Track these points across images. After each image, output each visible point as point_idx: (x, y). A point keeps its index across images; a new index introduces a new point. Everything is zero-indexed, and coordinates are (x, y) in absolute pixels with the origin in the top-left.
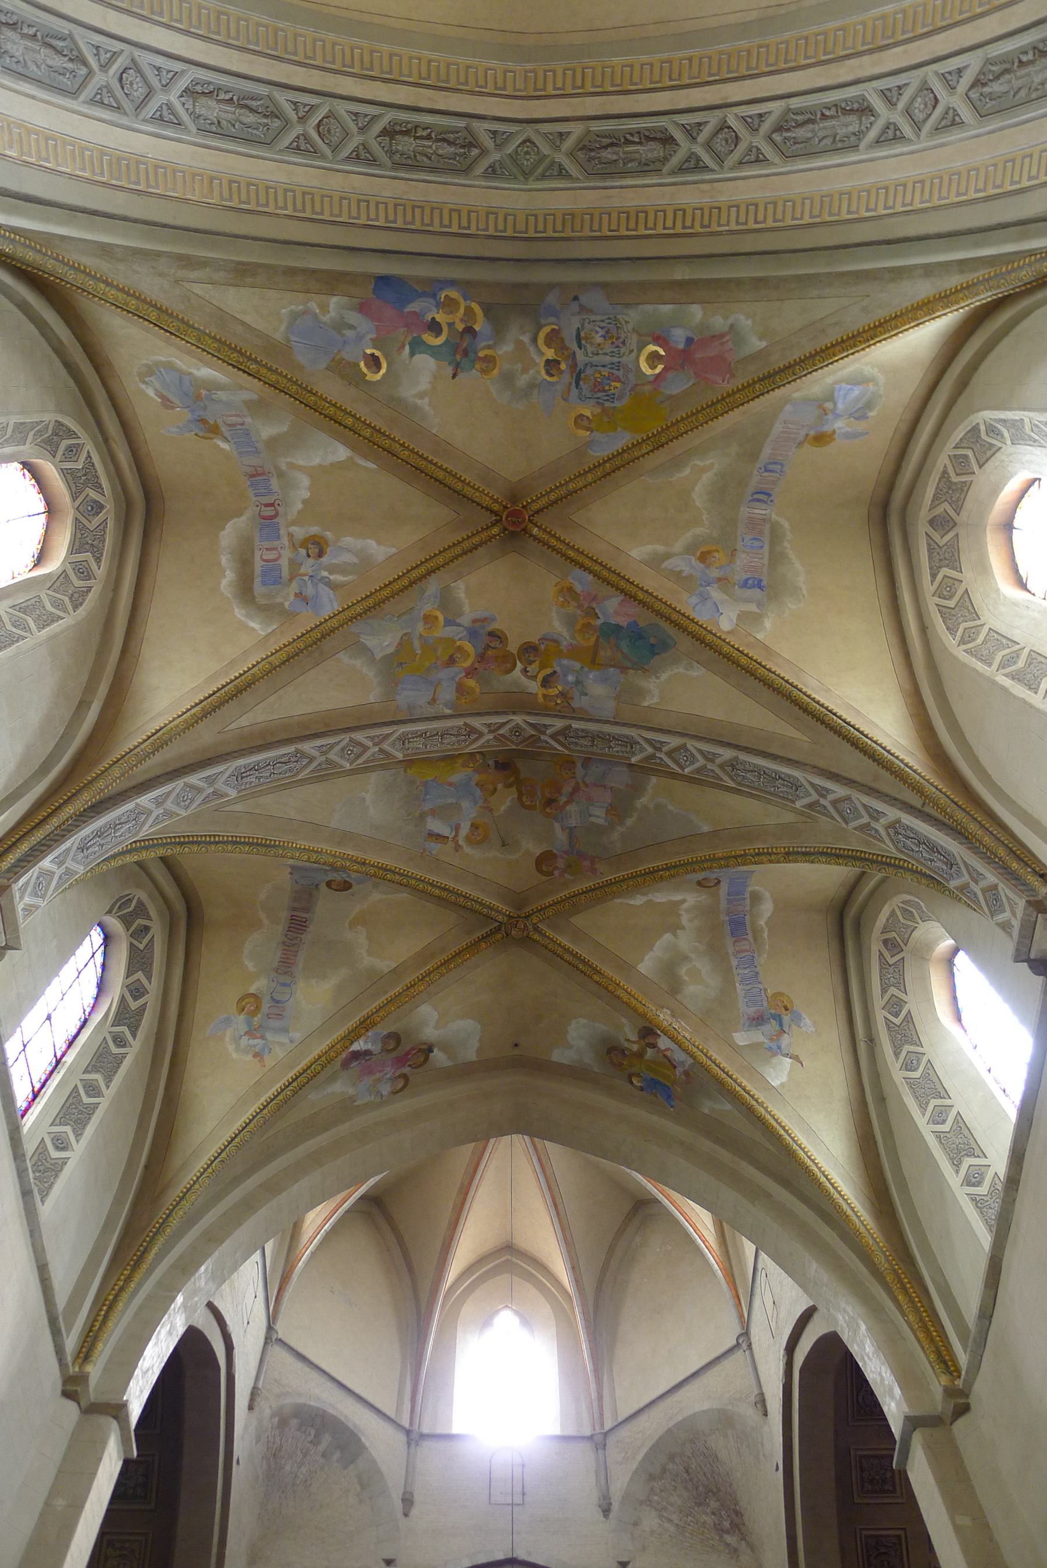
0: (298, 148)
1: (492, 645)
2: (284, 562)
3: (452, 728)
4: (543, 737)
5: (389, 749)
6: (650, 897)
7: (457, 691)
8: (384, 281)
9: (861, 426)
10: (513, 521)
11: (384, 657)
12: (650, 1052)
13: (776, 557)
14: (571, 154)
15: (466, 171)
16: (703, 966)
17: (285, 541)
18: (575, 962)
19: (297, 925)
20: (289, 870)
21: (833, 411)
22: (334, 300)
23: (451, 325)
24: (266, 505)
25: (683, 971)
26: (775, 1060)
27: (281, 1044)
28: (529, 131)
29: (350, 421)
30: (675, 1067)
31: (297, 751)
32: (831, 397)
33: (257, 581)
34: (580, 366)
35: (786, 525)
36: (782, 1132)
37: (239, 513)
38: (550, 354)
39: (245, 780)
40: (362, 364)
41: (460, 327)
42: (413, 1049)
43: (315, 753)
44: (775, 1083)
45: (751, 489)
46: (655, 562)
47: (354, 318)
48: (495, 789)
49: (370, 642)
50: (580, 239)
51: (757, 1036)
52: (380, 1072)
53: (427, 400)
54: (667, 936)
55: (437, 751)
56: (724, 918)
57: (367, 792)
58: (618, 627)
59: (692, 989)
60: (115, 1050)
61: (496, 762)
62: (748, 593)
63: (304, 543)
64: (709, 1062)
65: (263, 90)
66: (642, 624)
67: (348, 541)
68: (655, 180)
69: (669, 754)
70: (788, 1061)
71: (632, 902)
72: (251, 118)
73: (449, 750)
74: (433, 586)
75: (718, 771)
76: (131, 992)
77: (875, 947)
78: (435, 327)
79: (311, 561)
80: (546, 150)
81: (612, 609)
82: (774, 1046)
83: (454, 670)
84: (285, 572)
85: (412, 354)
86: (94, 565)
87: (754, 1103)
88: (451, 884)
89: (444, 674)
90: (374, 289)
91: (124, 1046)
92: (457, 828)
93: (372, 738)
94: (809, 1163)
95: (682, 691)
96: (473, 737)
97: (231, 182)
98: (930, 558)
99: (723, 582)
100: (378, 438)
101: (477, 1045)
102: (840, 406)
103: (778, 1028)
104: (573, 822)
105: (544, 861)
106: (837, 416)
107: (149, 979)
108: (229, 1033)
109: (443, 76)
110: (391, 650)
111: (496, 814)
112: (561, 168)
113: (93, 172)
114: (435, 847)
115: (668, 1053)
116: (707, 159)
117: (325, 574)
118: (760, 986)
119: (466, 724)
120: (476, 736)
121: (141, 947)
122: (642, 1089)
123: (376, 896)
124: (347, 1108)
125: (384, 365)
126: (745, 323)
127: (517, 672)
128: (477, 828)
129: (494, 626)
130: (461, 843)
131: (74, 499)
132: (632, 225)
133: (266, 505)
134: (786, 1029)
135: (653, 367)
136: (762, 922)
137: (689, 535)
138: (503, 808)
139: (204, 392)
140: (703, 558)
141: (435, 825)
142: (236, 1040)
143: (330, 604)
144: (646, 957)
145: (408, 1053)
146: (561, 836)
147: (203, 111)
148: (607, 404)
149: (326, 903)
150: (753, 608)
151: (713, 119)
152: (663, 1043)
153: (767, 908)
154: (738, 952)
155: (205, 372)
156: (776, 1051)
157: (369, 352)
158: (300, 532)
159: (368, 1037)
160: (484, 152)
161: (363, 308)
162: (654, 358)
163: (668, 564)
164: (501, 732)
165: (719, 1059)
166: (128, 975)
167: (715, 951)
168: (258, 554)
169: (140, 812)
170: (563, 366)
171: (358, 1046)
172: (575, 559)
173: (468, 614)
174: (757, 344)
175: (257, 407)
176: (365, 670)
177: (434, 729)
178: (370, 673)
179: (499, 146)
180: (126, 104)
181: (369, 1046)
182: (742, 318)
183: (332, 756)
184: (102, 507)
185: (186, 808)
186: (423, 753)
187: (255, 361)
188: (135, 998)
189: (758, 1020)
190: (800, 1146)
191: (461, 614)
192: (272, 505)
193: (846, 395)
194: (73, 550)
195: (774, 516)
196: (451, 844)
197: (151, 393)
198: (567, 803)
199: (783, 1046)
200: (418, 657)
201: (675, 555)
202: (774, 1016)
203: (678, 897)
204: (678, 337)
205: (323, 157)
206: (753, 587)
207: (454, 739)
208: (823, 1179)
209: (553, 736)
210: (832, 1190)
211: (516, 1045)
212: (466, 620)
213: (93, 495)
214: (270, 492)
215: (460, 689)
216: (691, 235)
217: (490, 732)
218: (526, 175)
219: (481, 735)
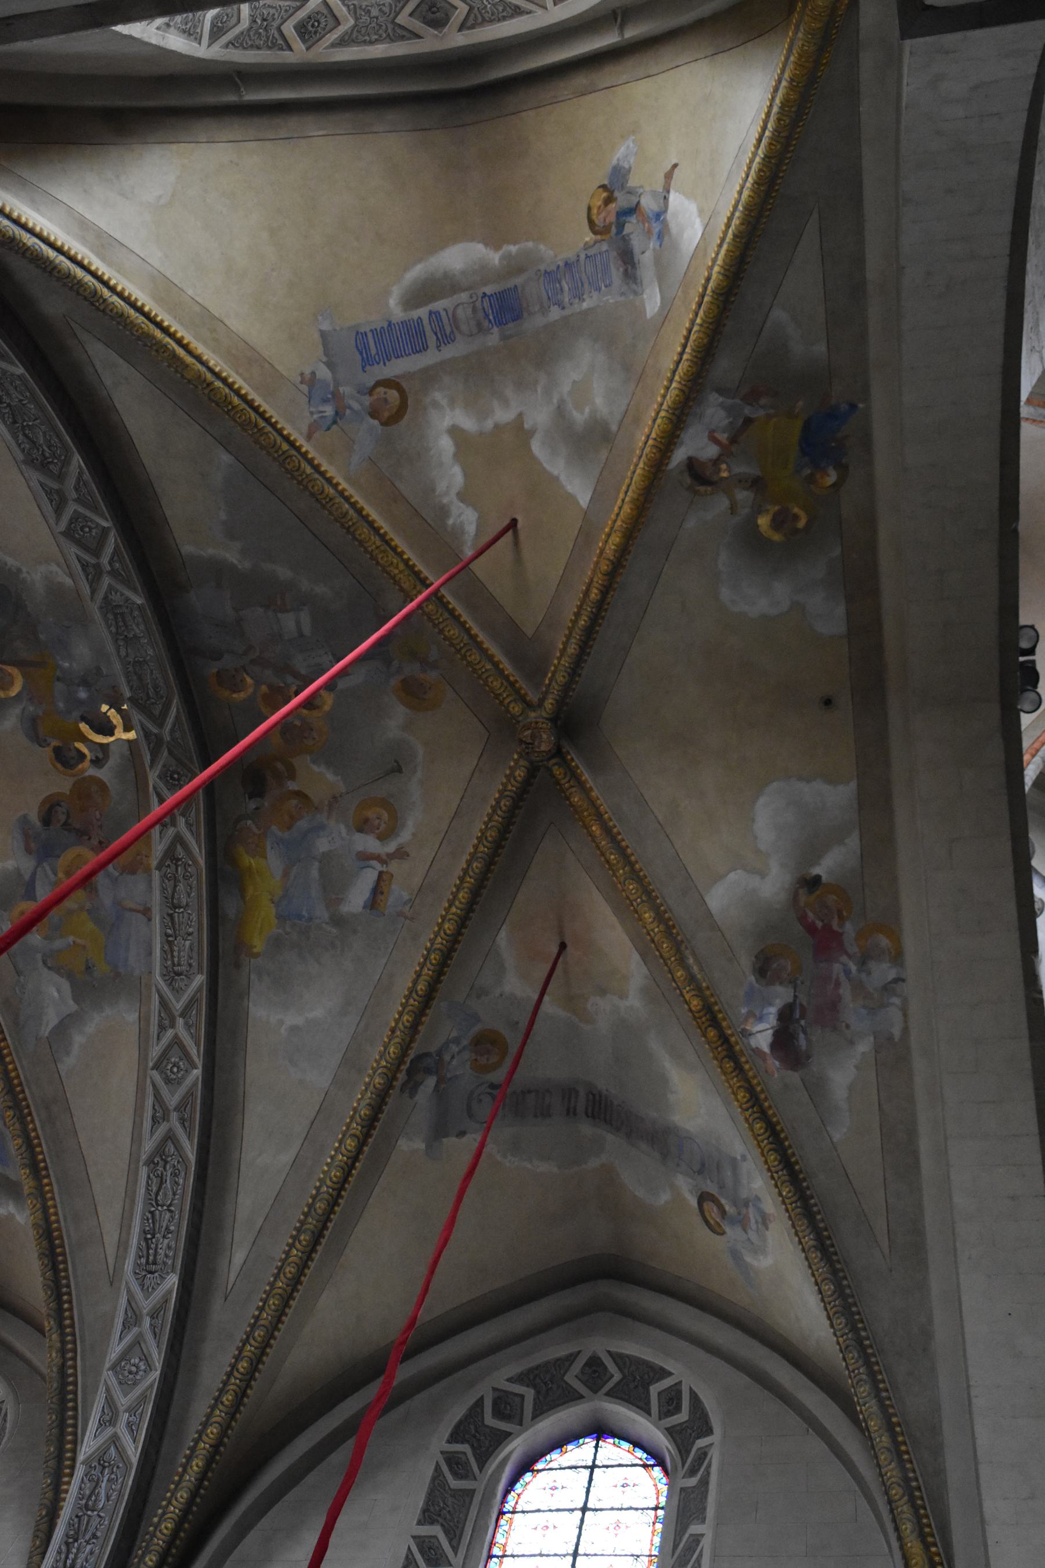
1: (63, 818)
3: (163, 890)
4: (167, 738)
5: (185, 998)
6: (450, 499)
11: (76, 999)
25: (580, 418)
30: (748, 421)
39: (160, 1258)
43: (162, 1130)
48: (298, 794)
49: (51, 1019)
52: (838, 984)
55: (200, 916)
56: (493, 338)
57: (281, 1022)
69: (97, 553)
73: (200, 896)
82: (656, 227)
92: (365, 857)
93: (162, 1028)
96: (180, 852)
101: (819, 786)
103: (633, 219)
110: (66, 986)
114: (398, 893)
115: (723, 437)
118: (583, 257)
120: (179, 847)
124: (893, 1057)
127: (103, 774)
128: (366, 821)
129: (34, 817)
130: (391, 847)
136: (495, 258)
138: (330, 776)
141: (356, 899)
144: (569, 488)
145: (811, 929)
149: (545, 1065)
152: (696, 444)
153: (458, 257)
159: (751, 1014)
166: (646, 1410)
167: (545, 354)
169: (100, 1461)
171: (762, 1036)
176: (90, 1028)
177: (162, 922)
178: (94, 1023)
181: (772, 1011)
185: (150, 1367)
186: (200, 942)
196: (394, 867)
200: (79, 941)
203: (446, 445)
207: (181, 887)
212: (26, 864)
219: (178, 839)
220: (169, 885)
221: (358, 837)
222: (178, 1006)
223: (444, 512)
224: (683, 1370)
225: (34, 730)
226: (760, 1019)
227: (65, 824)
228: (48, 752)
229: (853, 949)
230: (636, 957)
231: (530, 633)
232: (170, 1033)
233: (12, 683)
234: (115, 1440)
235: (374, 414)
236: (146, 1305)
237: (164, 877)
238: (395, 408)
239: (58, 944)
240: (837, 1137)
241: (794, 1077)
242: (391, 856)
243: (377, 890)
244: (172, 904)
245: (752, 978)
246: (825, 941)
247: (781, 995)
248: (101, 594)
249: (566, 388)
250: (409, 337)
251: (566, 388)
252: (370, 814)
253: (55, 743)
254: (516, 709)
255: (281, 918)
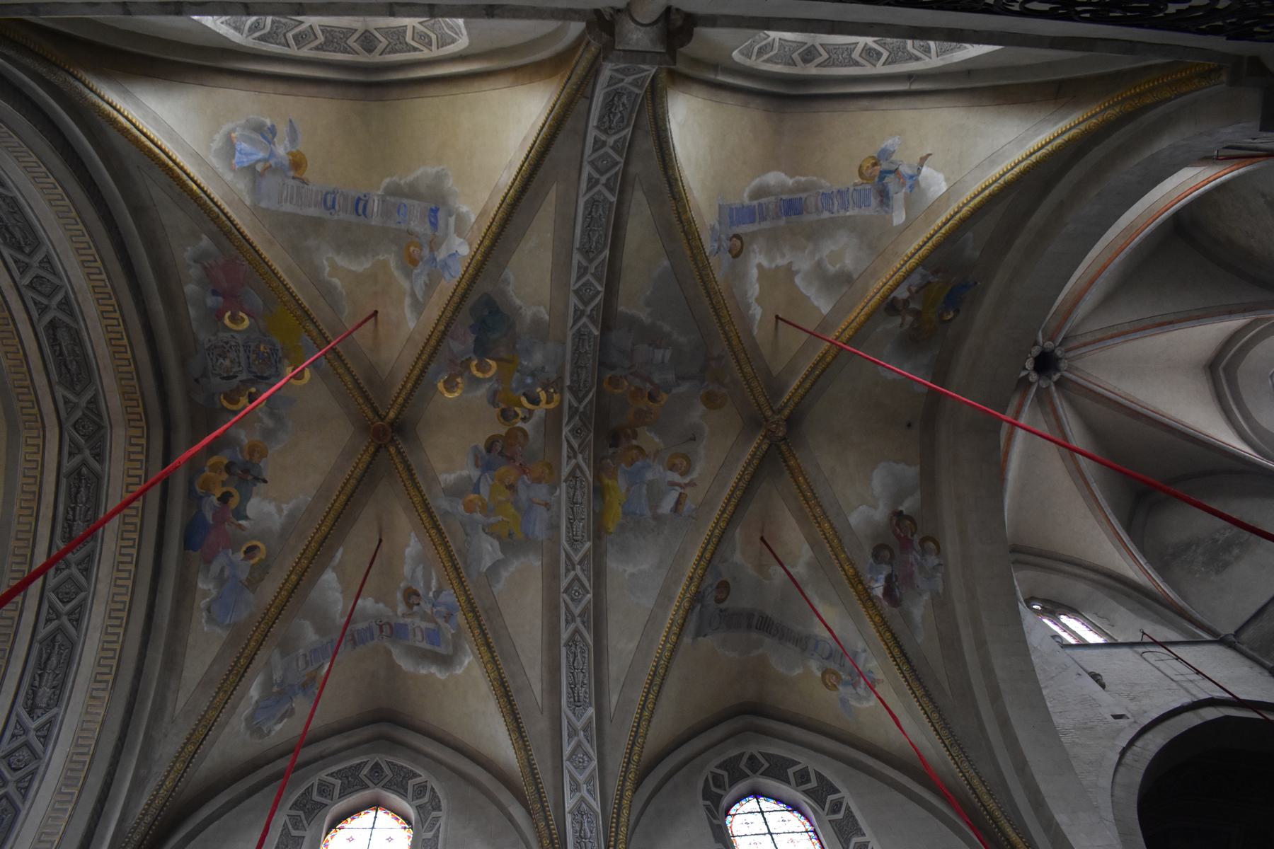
0: (77, 620)
2: (424, 625)
4: (581, 409)
5: (580, 554)
6: (752, 300)
7: (540, 482)
8: (189, 541)
9: (283, 129)
10: (386, 434)
11: (503, 550)
12: (912, 306)
13: (412, 192)
14: (78, 394)
15: (98, 478)
16: (828, 248)
17: (408, 620)
18: (812, 378)
19: (765, 625)
20: (700, 639)
21: (265, 160)
22: (201, 585)
23: (224, 484)
24: (381, 631)
25: (832, 269)
26: (923, 184)
27: (866, 659)
28: (68, 426)
29: (294, 577)
30: (929, 283)
31: (567, 645)
32: (251, 169)
33: (437, 649)
34: (251, 376)
35: (387, 180)
36: (987, 192)
37: (389, 653)
38: (244, 400)
40: (252, 562)
41: (225, 476)
42: (894, 531)
43: (572, 627)
44: (943, 187)
45: (353, 218)
46: (418, 307)
47: (215, 567)
48: (637, 447)
49: (487, 562)
50: (141, 387)
51: (898, 198)
53: (284, 506)
54: (798, 280)
58: (477, 341)
59: (849, 262)
60: (840, 816)
61: (611, 446)
62: (441, 223)
63: (410, 606)
64: (917, 256)
65: (36, 647)
66: (472, 322)
67: (407, 570)
68: (85, 334)
69: (586, 304)
70: (925, 170)
71: (758, 317)
72: (54, 660)
74: (441, 503)
75: (596, 263)
76: (802, 783)
77: (812, 70)
78: (225, 498)
79: (422, 603)
80: (79, 414)
81: (461, 344)
82: (909, 183)
83: (520, 486)
84: (431, 626)
85: (246, 518)
86: (418, 780)
87: (957, 217)
88: (728, 491)
89: (523, 495)
90: (194, 550)
91: (841, 804)
92: (673, 484)
93: (568, 571)
94: (1017, 170)
95: (532, 282)
96: (578, 473)
97: (96, 681)
98: (400, 51)
99: (434, 245)
100: (309, 554)
102: (261, 155)
103: (892, 176)
104: (671, 377)
105: (711, 401)
106: (272, 154)
107: (796, 763)
108: (853, 703)
109: (31, 497)
110: (496, 543)
111: (662, 446)
112: (90, 402)
113: (70, 802)
114: (689, 505)
115: (914, 289)
116: (59, 297)
117: (431, 594)
119: (566, 481)
121: (766, 765)
122: (957, 311)
123: (738, 557)
124: (941, 603)
125: (255, 543)
126: (189, 253)
127: (527, 427)
129: (482, 446)
130: (687, 480)
131: (367, 787)
132: (123, 349)
133: (381, 631)
134: (894, 167)
135: (243, 320)
136: (790, 182)
137: (396, 273)
138: (657, 440)
139: (275, 689)
140: (414, 262)
141: (667, 505)
142: (859, 698)
143: (449, 597)
144: (816, 303)
145: (898, 537)
146: (684, 388)
147: (45, 700)
148: (280, 354)
149: (741, 601)
150: (452, 220)
151: (29, 294)
152: (902, 293)
153: (774, 178)
154: (817, 209)
155: (254, 693)
156: (914, 177)
157: (242, 556)
158: (401, 608)
160: (84, 463)
161: (208, 562)
162: (234, 319)
163: (419, 296)
164: (576, 446)
165: (915, 245)
166: (787, 782)
167: (816, 233)
168: (418, 644)
169: (579, 812)
170: (253, 390)
171: (878, 589)
172: (420, 379)
173: (468, 471)
174: (205, 242)
175: (286, 648)
176: (512, 569)
178: (515, 565)
179: (80, 450)
180: (31, 767)
181: (882, 577)
182: (186, 255)
183: (577, 611)
184: (377, 764)
185: (590, 759)
187: (239, 658)
188: (809, 781)
189: (884, 197)
190: (1001, 176)
191: (470, 477)
192: (381, 627)
193: (247, 154)
194: (403, 795)
195: (380, 192)
196: (688, 491)
197: (279, 727)
198: (652, 383)
199: (910, 172)
201: (412, 288)
202: (882, 178)
203: (754, 272)
204: (211, 301)
205: (85, 599)
206: (436, 218)
207: (578, 493)
208: (1033, 158)
209: (580, 401)
210: (1044, 151)
211: (909, 425)
212: (475, 474)
213: (365, 771)
214: (370, 629)
215: (538, 480)
216: (119, 306)
217: (575, 457)
218: (100, 427)
219: (578, 466)
220: (571, 491)
221: (669, 473)
222: (577, 559)
223: (748, 306)
224: (805, 760)
225: (493, 399)
226: (877, 581)
227: (500, 453)
228: (498, 410)
229: (918, 548)
230: (807, 546)
231: (774, 374)
232: (572, 574)
233: (489, 370)
234: (582, 799)
235: (730, 251)
236: (579, 724)
237: (568, 487)
238: (738, 250)
239: (492, 520)
240: (919, 641)
241: (895, 611)
242: (687, 485)
243: (678, 503)
244: (573, 502)
245: (871, 560)
246: (906, 544)
247: (886, 570)
248: (576, 327)
249: (825, 252)
250: (749, 214)
251: (825, 252)
252: (677, 461)
253: (503, 406)
254: (769, 413)
255: (625, 514)
